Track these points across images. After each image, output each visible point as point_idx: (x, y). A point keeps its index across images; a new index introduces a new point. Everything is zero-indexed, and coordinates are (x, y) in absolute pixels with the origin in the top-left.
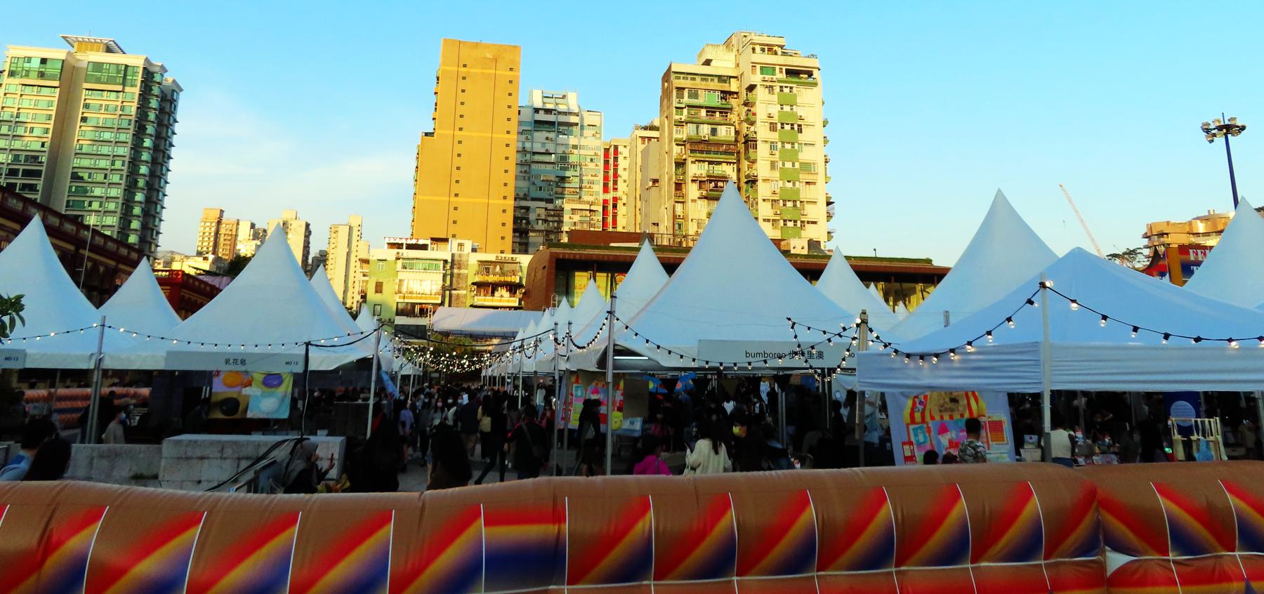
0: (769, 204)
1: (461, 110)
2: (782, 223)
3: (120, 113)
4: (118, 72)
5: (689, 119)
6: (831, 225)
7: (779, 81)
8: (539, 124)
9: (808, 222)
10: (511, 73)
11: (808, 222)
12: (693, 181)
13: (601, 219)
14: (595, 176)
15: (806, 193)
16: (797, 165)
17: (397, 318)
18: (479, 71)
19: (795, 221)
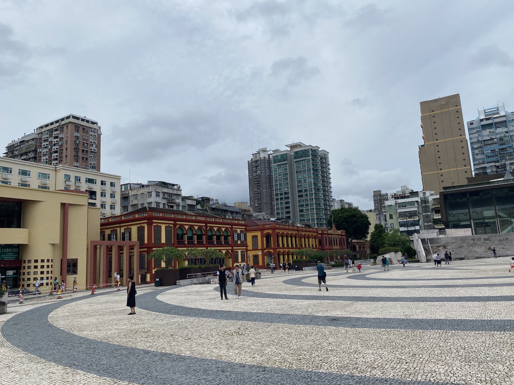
1: (435, 131)
4: (303, 153)
8: (484, 127)
10: (433, 113)
17: (400, 228)
18: (440, 111)
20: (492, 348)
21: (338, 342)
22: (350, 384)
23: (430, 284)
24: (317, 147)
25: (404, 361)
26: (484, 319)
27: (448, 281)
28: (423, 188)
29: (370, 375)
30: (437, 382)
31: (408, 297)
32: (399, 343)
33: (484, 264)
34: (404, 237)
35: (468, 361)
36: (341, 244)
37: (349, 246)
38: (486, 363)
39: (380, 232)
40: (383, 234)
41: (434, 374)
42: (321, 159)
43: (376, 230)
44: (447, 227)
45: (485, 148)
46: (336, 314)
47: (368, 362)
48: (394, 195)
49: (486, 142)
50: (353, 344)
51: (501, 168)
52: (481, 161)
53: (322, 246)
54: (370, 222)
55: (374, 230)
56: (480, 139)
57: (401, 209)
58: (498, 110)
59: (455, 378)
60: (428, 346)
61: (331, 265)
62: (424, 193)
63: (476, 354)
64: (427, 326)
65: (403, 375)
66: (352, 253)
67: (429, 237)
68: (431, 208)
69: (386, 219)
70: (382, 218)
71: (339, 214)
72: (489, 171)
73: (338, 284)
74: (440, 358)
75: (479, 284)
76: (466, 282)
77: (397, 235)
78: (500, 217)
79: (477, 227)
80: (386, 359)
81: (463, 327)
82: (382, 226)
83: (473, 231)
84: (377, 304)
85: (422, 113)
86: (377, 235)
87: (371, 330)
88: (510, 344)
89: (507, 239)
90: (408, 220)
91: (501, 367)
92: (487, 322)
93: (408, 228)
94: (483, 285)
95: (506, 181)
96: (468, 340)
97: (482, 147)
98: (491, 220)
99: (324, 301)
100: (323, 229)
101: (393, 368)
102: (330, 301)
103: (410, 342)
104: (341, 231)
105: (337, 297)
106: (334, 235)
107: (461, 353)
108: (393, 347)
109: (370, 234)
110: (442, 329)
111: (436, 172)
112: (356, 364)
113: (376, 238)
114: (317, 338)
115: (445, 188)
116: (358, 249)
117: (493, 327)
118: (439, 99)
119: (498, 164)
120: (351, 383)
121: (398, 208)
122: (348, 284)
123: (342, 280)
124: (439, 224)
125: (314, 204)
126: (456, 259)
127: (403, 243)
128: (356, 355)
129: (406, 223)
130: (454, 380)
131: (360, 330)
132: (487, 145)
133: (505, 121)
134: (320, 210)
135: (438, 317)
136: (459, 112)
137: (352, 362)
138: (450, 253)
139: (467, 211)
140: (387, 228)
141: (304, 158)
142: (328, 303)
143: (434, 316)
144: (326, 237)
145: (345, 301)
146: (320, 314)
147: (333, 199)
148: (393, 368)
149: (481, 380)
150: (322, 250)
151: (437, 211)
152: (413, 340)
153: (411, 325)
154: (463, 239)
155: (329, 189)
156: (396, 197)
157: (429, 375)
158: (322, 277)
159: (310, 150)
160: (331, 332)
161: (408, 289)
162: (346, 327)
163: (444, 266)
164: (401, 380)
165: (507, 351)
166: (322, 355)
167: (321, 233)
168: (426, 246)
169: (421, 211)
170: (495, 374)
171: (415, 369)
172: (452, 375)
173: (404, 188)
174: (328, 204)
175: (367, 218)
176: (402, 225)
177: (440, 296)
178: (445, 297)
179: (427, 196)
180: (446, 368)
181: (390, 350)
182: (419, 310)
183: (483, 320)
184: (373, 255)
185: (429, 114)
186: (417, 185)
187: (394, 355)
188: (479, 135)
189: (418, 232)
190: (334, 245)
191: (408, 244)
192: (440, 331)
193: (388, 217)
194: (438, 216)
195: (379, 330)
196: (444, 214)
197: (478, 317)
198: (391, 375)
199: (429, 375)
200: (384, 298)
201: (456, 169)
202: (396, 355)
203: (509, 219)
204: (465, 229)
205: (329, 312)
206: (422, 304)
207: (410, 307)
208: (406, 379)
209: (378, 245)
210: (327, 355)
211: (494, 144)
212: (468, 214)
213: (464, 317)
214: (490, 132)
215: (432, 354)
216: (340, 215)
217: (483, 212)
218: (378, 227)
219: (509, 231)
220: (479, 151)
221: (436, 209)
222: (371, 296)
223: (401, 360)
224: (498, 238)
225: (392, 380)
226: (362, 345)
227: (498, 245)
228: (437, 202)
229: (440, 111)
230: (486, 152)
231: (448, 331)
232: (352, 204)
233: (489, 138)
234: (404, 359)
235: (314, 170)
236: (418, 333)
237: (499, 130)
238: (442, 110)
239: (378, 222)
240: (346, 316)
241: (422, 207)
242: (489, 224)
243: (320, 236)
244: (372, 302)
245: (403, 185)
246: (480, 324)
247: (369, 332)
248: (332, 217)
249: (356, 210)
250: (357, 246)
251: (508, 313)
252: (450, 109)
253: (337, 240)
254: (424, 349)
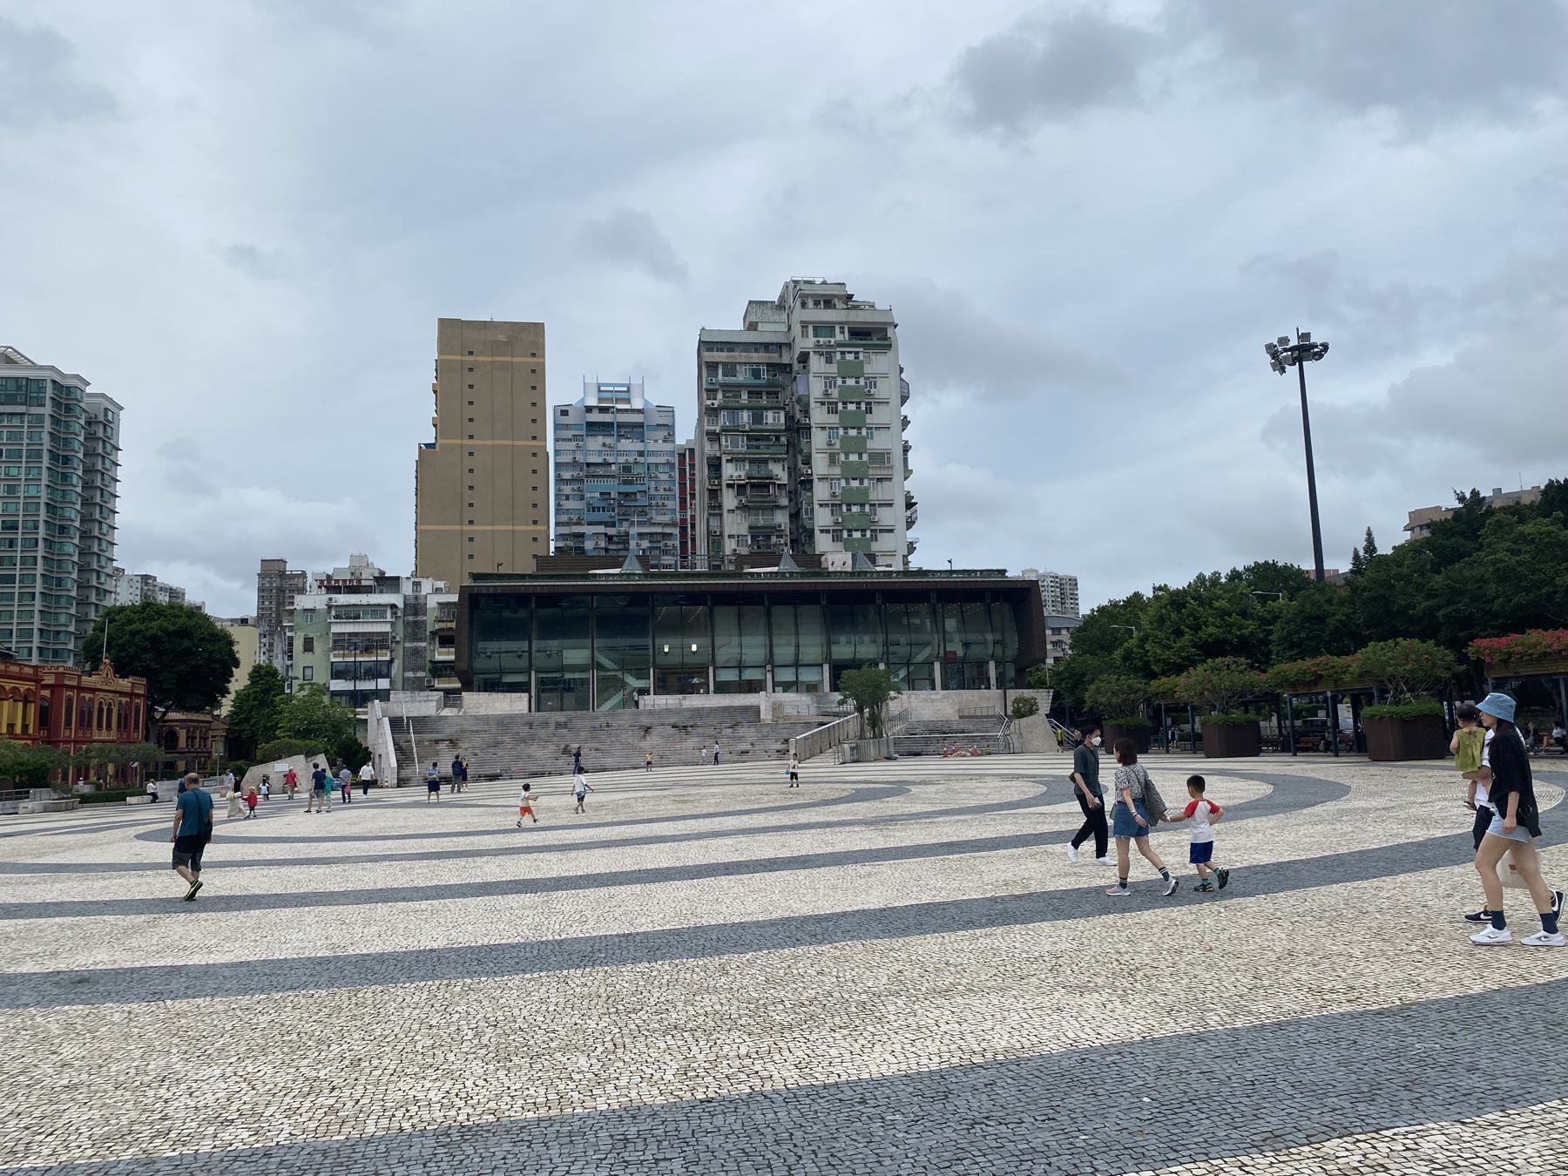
0: (828, 510)
1: (470, 412)
4: (19, 388)
5: (724, 404)
6: (911, 535)
8: (593, 428)
9: (881, 531)
10: (471, 358)
11: (881, 531)
12: (729, 486)
13: (677, 543)
14: (670, 490)
15: (878, 493)
16: (865, 457)
17: (333, 682)
18: (489, 359)
19: (863, 531)
20: (563, 1014)
23: (405, 849)
24: (78, 377)
25: (325, 1084)
26: (544, 939)
27: (455, 839)
29: (215, 1147)
30: (421, 1131)
31: (342, 890)
32: (311, 1033)
33: (549, 790)
34: (342, 710)
35: (503, 1057)
36: (123, 724)
38: (547, 1057)
39: (266, 691)
40: (274, 696)
42: (89, 423)
43: (253, 683)
44: (468, 686)
46: (91, 962)
47: (206, 1107)
49: (592, 469)
50: (154, 1057)
51: (617, 543)
52: (575, 517)
53: (49, 731)
54: (237, 656)
55: (249, 682)
56: (580, 458)
58: (628, 391)
59: (470, 1111)
60: (397, 1030)
62: (417, 584)
63: (525, 1036)
64: (396, 972)
65: (322, 1129)
66: (162, 756)
70: (279, 647)
71: (130, 622)
72: (589, 545)
73: (99, 861)
74: (430, 1061)
76: (503, 840)
77: (321, 702)
78: (600, 667)
80: (267, 1087)
81: (492, 965)
83: (533, 699)
84: (240, 917)
85: (441, 350)
86: (255, 699)
87: (219, 1003)
88: (605, 999)
90: (358, 659)
91: (583, 1061)
92: (552, 947)
93: (357, 682)
95: (625, 577)
96: (504, 1000)
97: (580, 480)
98: (577, 676)
99: (42, 921)
100: (61, 670)
101: (290, 1112)
102: (69, 920)
103: (344, 1024)
104: (131, 679)
105: (97, 903)
106: (102, 694)
107: (488, 1036)
108: (291, 1047)
109: (232, 696)
110: (438, 978)
111: (458, 527)
112: (164, 1118)
114: (14, 1053)
115: (476, 577)
116: (182, 743)
117: (567, 957)
118: (491, 323)
119: (611, 531)
121: (333, 620)
122: (139, 857)
123: (115, 846)
124: (446, 676)
126: (479, 778)
127: (333, 726)
128: (162, 1091)
129: (352, 669)
130: (468, 1115)
131: (181, 1005)
133: (641, 425)
134: (58, 602)
135: (428, 943)
136: (537, 373)
137: (148, 1114)
139: (524, 645)
140: (292, 678)
141: (22, 409)
142: (60, 925)
143: (416, 943)
144: (70, 700)
145: (128, 914)
146: (27, 968)
147: (117, 569)
148: (290, 1112)
150: (49, 743)
151: (446, 640)
152: (354, 1018)
153: (350, 975)
154: (505, 722)
155: (105, 531)
156: (331, 586)
157: (399, 1114)
159: (49, 386)
160: (69, 1026)
161: (342, 867)
162: (128, 1001)
164: (313, 1144)
165: (596, 1018)
166: (32, 1109)
167: (52, 682)
168: (401, 737)
169: (402, 635)
170: (569, 1082)
171: (357, 1103)
172: (461, 1104)
173: (360, 561)
174: (94, 583)
175: (231, 643)
176: (337, 674)
177: (435, 882)
178: (445, 886)
179: (423, 593)
182: (374, 929)
186: (398, 558)
187: (292, 1070)
188: (578, 446)
189: (383, 695)
190: (100, 726)
191: (351, 731)
192: (431, 983)
193: (298, 645)
194: (445, 655)
195: (245, 1001)
197: (532, 936)
198: (285, 1134)
200: (263, 896)
203: (619, 674)
204: (513, 694)
206: (382, 909)
207: (347, 921)
208: (328, 1138)
209: (253, 732)
212: (527, 654)
214: (604, 445)
215: (409, 1050)
216: (136, 626)
217: (564, 652)
218: (265, 678)
221: (441, 634)
224: (588, 723)
225: (286, 1150)
226: (186, 1056)
227: (586, 741)
229: (489, 359)
230: (589, 495)
231: (453, 982)
232: (183, 594)
233: (600, 460)
235: (53, 456)
236: (369, 995)
237: (625, 444)
239: (263, 658)
240: (128, 965)
241: (406, 624)
243: (47, 693)
245: (356, 553)
246: (535, 952)
248: (103, 631)
249: (195, 612)
250: (182, 734)
251: (601, 918)
252: (515, 359)
253: (110, 711)
254: (387, 1040)
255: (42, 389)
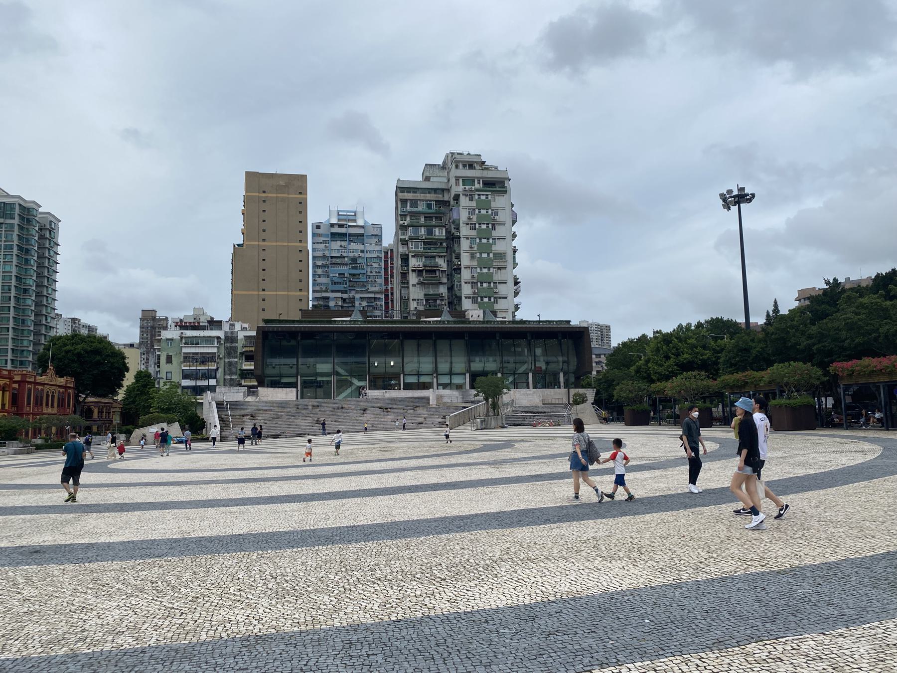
0: (469, 286)
1: (263, 226)
2: (479, 299)
3: (365, 266)
7: (477, 190)
8: (335, 236)
10: (264, 195)
11: (500, 298)
12: (413, 271)
13: (383, 303)
16: (491, 255)
18: (275, 195)
20: (315, 571)
21: (44, 596)
22: (69, 671)
24: (34, 202)
25: (177, 611)
26: (305, 528)
27: (253, 471)
28: (230, 316)
29: (113, 647)
30: (232, 638)
32: (169, 582)
34: (189, 397)
35: (280, 596)
36: (61, 404)
37: (78, 409)
38: (306, 596)
39: (145, 386)
40: (149, 389)
41: (228, 625)
42: (41, 229)
43: (137, 381)
44: (261, 384)
45: (331, 269)
47: (108, 624)
48: (178, 321)
49: (334, 260)
50: (78, 595)
52: (324, 288)
53: (17, 407)
55: (134, 381)
56: (327, 253)
57: (189, 348)
58: (355, 215)
59: (261, 627)
60: (219, 580)
61: (35, 445)
62: (232, 325)
63: (293, 584)
65: (175, 637)
66: (84, 423)
67: (231, 400)
68: (239, 351)
69: (159, 363)
70: (152, 361)
71: (65, 345)
72: (332, 304)
74: (238, 598)
75: (300, 475)
77: (177, 392)
78: (338, 374)
79: (305, 387)
81: (274, 543)
82: (149, 375)
83: (299, 392)
84: (128, 515)
87: (116, 565)
88: (339, 563)
89: (342, 408)
90: (198, 368)
91: (326, 598)
94: (306, 476)
96: (281, 563)
97: (328, 267)
98: (325, 379)
100: (24, 372)
101: (156, 627)
102: (28, 517)
103: (188, 577)
104: (65, 378)
105: (45, 507)
106: (48, 387)
107: (272, 584)
108: (157, 590)
109: (125, 388)
110: (243, 550)
112: (83, 631)
113: (136, 397)
115: (267, 321)
116: (95, 415)
117: (318, 539)
118: (276, 174)
119: (345, 296)
120: (72, 668)
121: (183, 345)
125: (11, 319)
126: (268, 437)
127: (184, 406)
128: (82, 615)
129: (195, 373)
130: (260, 629)
132: (335, 264)
133: (362, 235)
134: (22, 333)
136: (302, 206)
138: (261, 426)
139: (294, 361)
140: (160, 378)
143: (230, 530)
144: (30, 390)
148: (156, 627)
149: (298, 622)
151: (249, 357)
152: (194, 573)
153: (192, 548)
154: (283, 405)
155: (50, 292)
156: (182, 325)
158: (72, 471)
159: (17, 207)
160: (28, 578)
161: (188, 487)
162: (62, 563)
163: (249, 447)
165: (334, 574)
166: (6, 625)
167: (19, 379)
168: (223, 413)
169: (223, 355)
173: (199, 311)
175: (124, 358)
176: (186, 376)
179: (236, 330)
180: (247, 613)
181: (151, 595)
182: (206, 522)
183: (303, 531)
184: (124, 428)
185: (257, 194)
186: (222, 310)
187: (158, 603)
189: (212, 389)
190: (47, 405)
192: (239, 553)
193: (163, 360)
194: (249, 366)
195: (131, 563)
196: (260, 363)
197: (297, 527)
198: (153, 640)
199: (220, 628)
200: (142, 504)
201: (286, 293)
202: (164, 603)
203: (349, 378)
204: (288, 389)
205: (26, 537)
206: (211, 511)
207: (191, 518)
208: (179, 642)
209: (137, 409)
210: (19, 624)
211: (343, 264)
213: (276, 528)
214: (341, 246)
215: (226, 592)
216: (68, 348)
218: (144, 378)
219: (345, 398)
220: (323, 272)
222: (118, 502)
223: (173, 611)
224: (331, 406)
227: (329, 416)
228: (250, 343)
229: (275, 195)
230: (332, 275)
231: (252, 553)
232: (96, 329)
233: (338, 255)
234: (177, 609)
235: (20, 248)
237: (353, 246)
238: (279, 193)
239: (143, 367)
240: (63, 543)
241: (226, 348)
242: (322, 384)
243: (16, 386)
244: (120, 514)
245: (197, 307)
246: (299, 536)
247: (111, 569)
249: (103, 340)
250: (96, 410)
251: (338, 517)
252: (290, 196)
253: (53, 396)
254: (213, 586)
255: (13, 209)
